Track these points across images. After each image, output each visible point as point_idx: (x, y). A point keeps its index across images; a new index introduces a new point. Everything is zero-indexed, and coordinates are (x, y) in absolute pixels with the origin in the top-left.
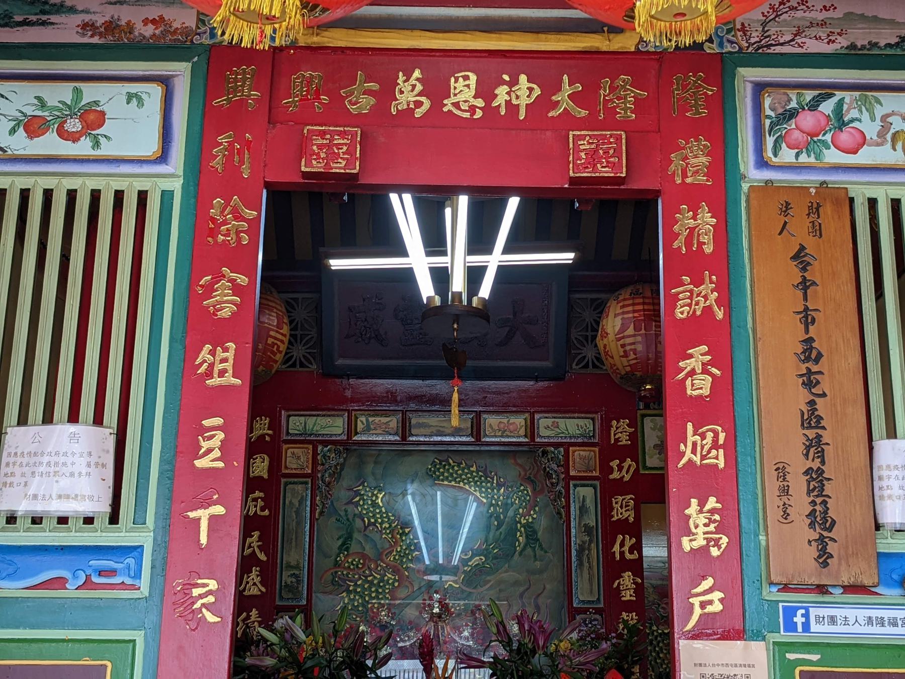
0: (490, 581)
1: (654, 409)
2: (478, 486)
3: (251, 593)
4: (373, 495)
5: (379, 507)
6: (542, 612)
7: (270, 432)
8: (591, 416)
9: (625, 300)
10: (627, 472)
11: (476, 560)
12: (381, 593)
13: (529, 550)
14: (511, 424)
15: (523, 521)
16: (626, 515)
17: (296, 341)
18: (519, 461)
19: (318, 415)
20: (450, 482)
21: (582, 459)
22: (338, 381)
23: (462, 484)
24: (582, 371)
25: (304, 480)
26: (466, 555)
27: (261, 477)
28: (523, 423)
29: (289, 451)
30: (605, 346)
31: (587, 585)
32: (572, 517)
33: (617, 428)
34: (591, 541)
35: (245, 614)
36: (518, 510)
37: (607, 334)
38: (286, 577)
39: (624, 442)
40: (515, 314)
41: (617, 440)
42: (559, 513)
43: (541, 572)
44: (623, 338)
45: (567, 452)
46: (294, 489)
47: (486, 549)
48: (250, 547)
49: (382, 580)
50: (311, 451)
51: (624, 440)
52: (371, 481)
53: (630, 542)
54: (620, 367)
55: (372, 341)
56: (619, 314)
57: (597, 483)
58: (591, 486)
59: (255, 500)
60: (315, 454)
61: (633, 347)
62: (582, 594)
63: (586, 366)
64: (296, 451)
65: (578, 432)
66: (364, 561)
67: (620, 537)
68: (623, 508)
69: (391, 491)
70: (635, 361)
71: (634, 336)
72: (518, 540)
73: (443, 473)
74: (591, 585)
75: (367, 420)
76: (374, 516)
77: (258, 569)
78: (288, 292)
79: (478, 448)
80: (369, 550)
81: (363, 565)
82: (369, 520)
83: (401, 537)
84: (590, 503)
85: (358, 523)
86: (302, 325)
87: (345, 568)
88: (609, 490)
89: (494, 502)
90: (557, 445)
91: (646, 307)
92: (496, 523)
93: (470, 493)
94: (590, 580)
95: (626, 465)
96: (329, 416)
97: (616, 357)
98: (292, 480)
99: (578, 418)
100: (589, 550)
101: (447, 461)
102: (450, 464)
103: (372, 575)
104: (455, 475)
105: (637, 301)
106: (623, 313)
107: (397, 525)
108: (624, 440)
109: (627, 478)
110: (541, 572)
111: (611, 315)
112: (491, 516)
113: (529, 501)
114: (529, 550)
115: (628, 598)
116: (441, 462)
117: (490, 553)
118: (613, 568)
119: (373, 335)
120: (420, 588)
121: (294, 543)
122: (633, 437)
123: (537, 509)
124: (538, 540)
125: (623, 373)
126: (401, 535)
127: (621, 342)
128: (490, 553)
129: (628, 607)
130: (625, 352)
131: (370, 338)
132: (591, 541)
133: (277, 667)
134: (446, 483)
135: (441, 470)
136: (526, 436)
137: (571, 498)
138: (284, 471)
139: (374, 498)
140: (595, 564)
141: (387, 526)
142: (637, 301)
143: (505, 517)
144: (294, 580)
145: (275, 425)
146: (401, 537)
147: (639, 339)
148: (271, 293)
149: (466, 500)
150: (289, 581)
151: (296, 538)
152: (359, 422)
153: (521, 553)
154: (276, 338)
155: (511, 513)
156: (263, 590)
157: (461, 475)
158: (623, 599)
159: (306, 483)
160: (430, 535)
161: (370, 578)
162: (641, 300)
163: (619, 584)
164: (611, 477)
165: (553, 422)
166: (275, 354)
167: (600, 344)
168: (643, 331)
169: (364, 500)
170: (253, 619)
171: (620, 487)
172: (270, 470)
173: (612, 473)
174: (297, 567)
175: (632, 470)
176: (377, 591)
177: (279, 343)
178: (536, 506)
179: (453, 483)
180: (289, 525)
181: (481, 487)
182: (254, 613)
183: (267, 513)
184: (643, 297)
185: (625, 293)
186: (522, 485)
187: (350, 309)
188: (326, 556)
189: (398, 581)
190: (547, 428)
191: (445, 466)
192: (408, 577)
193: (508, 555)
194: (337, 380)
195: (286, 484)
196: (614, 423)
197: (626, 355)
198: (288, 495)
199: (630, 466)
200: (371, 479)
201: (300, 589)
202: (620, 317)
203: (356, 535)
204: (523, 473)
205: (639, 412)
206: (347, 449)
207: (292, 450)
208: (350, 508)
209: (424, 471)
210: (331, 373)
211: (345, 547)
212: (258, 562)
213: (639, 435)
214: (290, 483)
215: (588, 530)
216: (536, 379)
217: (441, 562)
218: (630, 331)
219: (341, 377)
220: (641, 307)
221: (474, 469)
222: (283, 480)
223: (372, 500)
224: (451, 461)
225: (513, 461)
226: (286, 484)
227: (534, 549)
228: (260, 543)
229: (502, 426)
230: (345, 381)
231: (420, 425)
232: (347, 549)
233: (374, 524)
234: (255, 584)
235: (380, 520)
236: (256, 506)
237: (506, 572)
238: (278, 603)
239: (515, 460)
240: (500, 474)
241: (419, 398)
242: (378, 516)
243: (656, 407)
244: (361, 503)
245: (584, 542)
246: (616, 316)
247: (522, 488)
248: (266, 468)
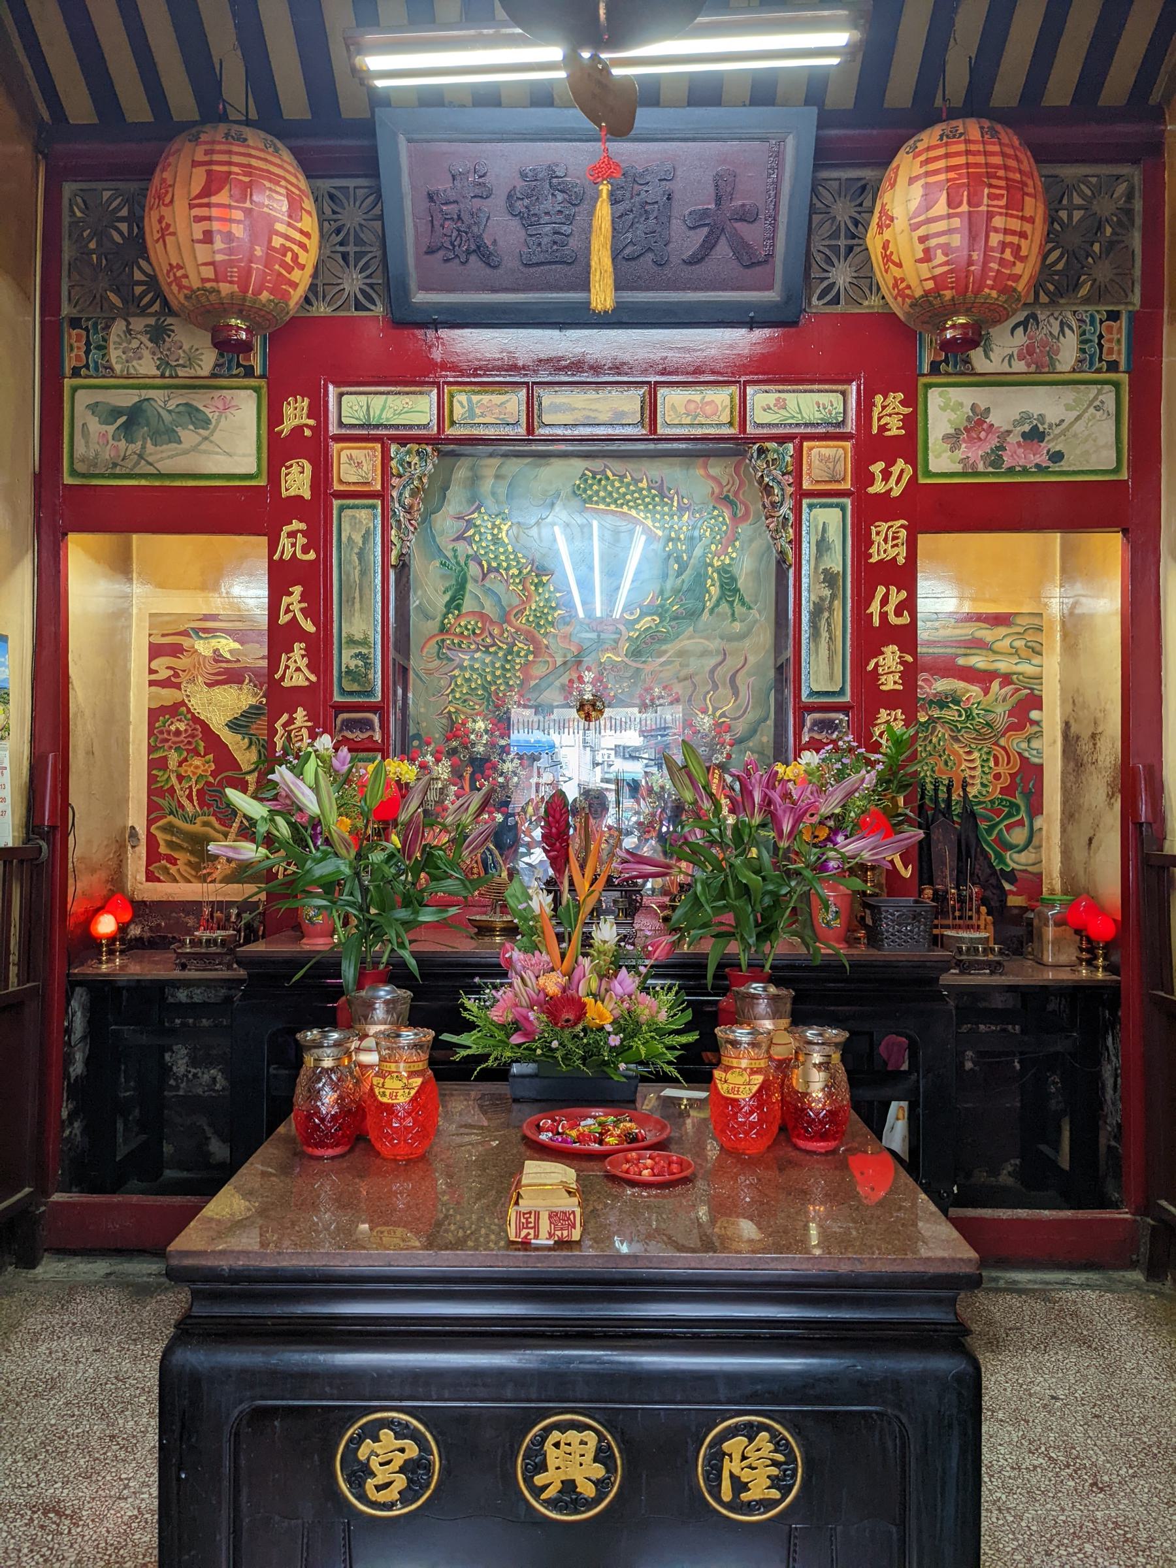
0: (665, 652)
1: (948, 374)
2: (649, 511)
3: (294, 683)
4: (494, 526)
5: (505, 545)
6: (741, 695)
7: (312, 422)
8: (840, 387)
9: (929, 149)
10: (897, 482)
11: (646, 622)
12: (508, 670)
14: (708, 403)
15: (717, 563)
16: (892, 553)
17: (367, 277)
18: (712, 471)
19: (388, 393)
20: (608, 505)
21: (827, 461)
22: (419, 333)
23: (625, 509)
24: (829, 309)
25: (371, 501)
26: (632, 614)
27: (299, 498)
28: (727, 402)
29: (344, 454)
30: (885, 246)
31: (824, 667)
32: (805, 558)
33: (884, 408)
34: (833, 597)
35: (285, 717)
36: (709, 546)
37: (892, 219)
38: (347, 658)
39: (894, 432)
40: (718, 200)
41: (883, 428)
42: (115, 465)
43: (742, 636)
44: (929, 221)
45: (799, 451)
46: (354, 517)
47: (662, 606)
48: (288, 611)
49: (510, 652)
50: (379, 454)
51: (895, 428)
52: (490, 504)
53: (897, 596)
54: (914, 283)
55: (473, 258)
56: (917, 178)
57: (848, 501)
58: (837, 506)
59: (292, 535)
60: (386, 458)
61: (942, 240)
62: (817, 681)
63: (836, 301)
64: (354, 453)
65: (818, 415)
66: (484, 624)
67: (881, 590)
68: (887, 542)
69: (521, 520)
70: (945, 268)
71: (949, 216)
72: (708, 591)
73: (597, 492)
75: (469, 401)
76: (496, 557)
77: (303, 645)
78: (332, 177)
79: (651, 446)
80: (489, 609)
81: (483, 630)
82: (489, 564)
83: (536, 589)
84: (834, 535)
85: (474, 570)
86: (356, 235)
87: (456, 635)
88: (868, 511)
89: (673, 535)
90: (782, 439)
91: (972, 159)
92: (676, 566)
93: (636, 521)
94: (831, 659)
95: (895, 470)
96: (407, 393)
97: (908, 263)
98: (351, 502)
99: (819, 391)
100: (831, 609)
101: (603, 472)
102: (607, 478)
103: (495, 644)
104: (615, 495)
105: (954, 149)
106: (927, 174)
107: (531, 571)
108: (895, 428)
109: (896, 492)
110: (742, 636)
111: (902, 180)
112: (669, 556)
113: (726, 532)
114: (724, 606)
115: (890, 686)
116: (594, 474)
117: (667, 611)
118: (868, 639)
119: (473, 247)
120: (565, 663)
121: (357, 606)
122: (910, 422)
123: (737, 543)
124: (739, 590)
125: (918, 293)
126: (536, 585)
127: (921, 232)
128: (667, 611)
129: (891, 700)
130: (927, 251)
131: (468, 252)
132: (833, 597)
133: (267, 863)
134: (602, 506)
135: (595, 487)
136: (731, 424)
137: (804, 528)
138: (337, 487)
139: (496, 531)
140: (839, 633)
141: (516, 572)
142: (954, 149)
143: (690, 558)
144: (360, 663)
145: (318, 410)
146: (536, 589)
147: (956, 222)
148: (276, 150)
149: (631, 532)
150: (353, 664)
151: (361, 597)
152: (455, 403)
153: (712, 611)
154: (287, 238)
155: (698, 552)
156: (313, 678)
157: (625, 494)
158: (883, 688)
159: (374, 507)
160: (585, 585)
161: (491, 650)
162: (962, 147)
163: (877, 665)
164: (871, 490)
165: (778, 400)
166: (290, 270)
167: (874, 241)
168: (964, 208)
169: (481, 534)
170: (298, 723)
171: (884, 508)
172: (314, 486)
173: (872, 484)
174: (364, 643)
175: (906, 478)
176: (503, 668)
177: (295, 248)
178: (737, 539)
179: (613, 507)
180: (348, 575)
181: (654, 512)
182: (300, 714)
183: (312, 556)
184: (967, 142)
185: (929, 137)
186: (715, 508)
187: (431, 197)
188: (428, 617)
189: (533, 653)
190: (766, 409)
191: (600, 480)
192: (547, 647)
193: (693, 614)
194: (417, 332)
195: (342, 509)
196: (879, 399)
197: (928, 256)
198: (346, 526)
199: (902, 471)
200: (490, 502)
201: (371, 676)
202: (922, 182)
203: (470, 586)
204: (717, 491)
205: (922, 380)
206: (439, 451)
207: (348, 452)
208: (461, 547)
209: (569, 489)
210: (409, 321)
211: (454, 603)
212: (303, 635)
213: (920, 418)
214: (349, 507)
215: (830, 579)
216: (751, 325)
217: (598, 614)
218: (941, 207)
219: (423, 325)
220: (962, 160)
221: (644, 484)
222: (336, 503)
223: (493, 534)
224: (609, 474)
225: (702, 472)
226: (342, 509)
227: (731, 603)
228: (304, 605)
229: (692, 406)
230: (430, 333)
231: (557, 409)
232: (458, 607)
233: (497, 570)
234: (298, 669)
235: (505, 564)
236: (294, 545)
237: (689, 638)
238: (337, 698)
239: (705, 467)
240: (683, 492)
241: (555, 364)
242: (502, 557)
243: (950, 370)
244: (477, 538)
245: (822, 599)
246: (912, 181)
247: (716, 513)
248: (308, 483)
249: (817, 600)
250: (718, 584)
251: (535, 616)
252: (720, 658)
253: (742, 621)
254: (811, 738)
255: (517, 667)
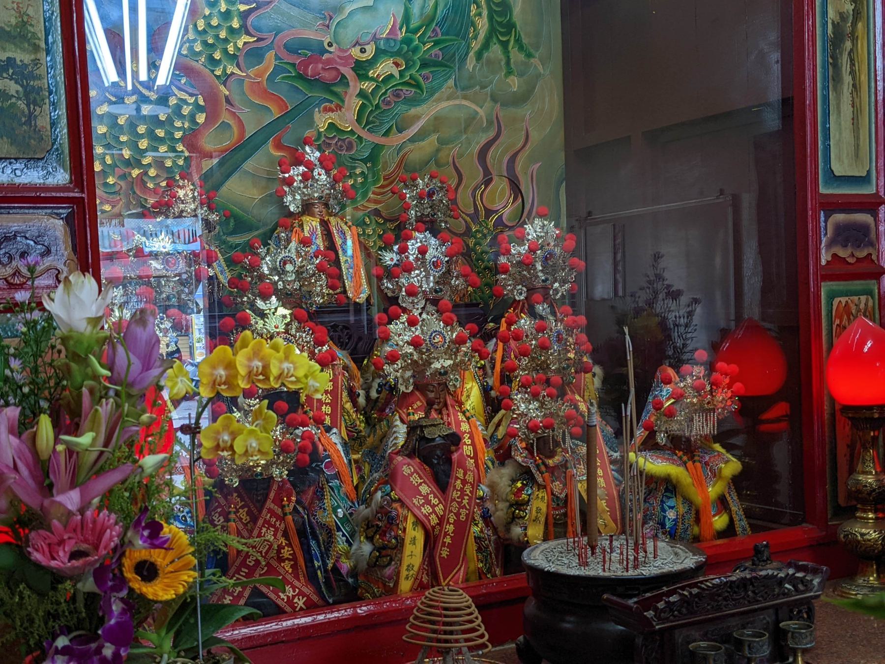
12: (161, 140)
13: (496, 50)
47: (407, 41)
72: (473, 24)
74: (857, 138)
100: (854, 39)
114: (496, 50)
201: (43, 122)
227: (505, 45)
249: (837, 19)
250: (485, 13)
251: (205, 43)
252: (492, 134)
253: (521, 75)
254: (835, 256)
255: (178, 135)
